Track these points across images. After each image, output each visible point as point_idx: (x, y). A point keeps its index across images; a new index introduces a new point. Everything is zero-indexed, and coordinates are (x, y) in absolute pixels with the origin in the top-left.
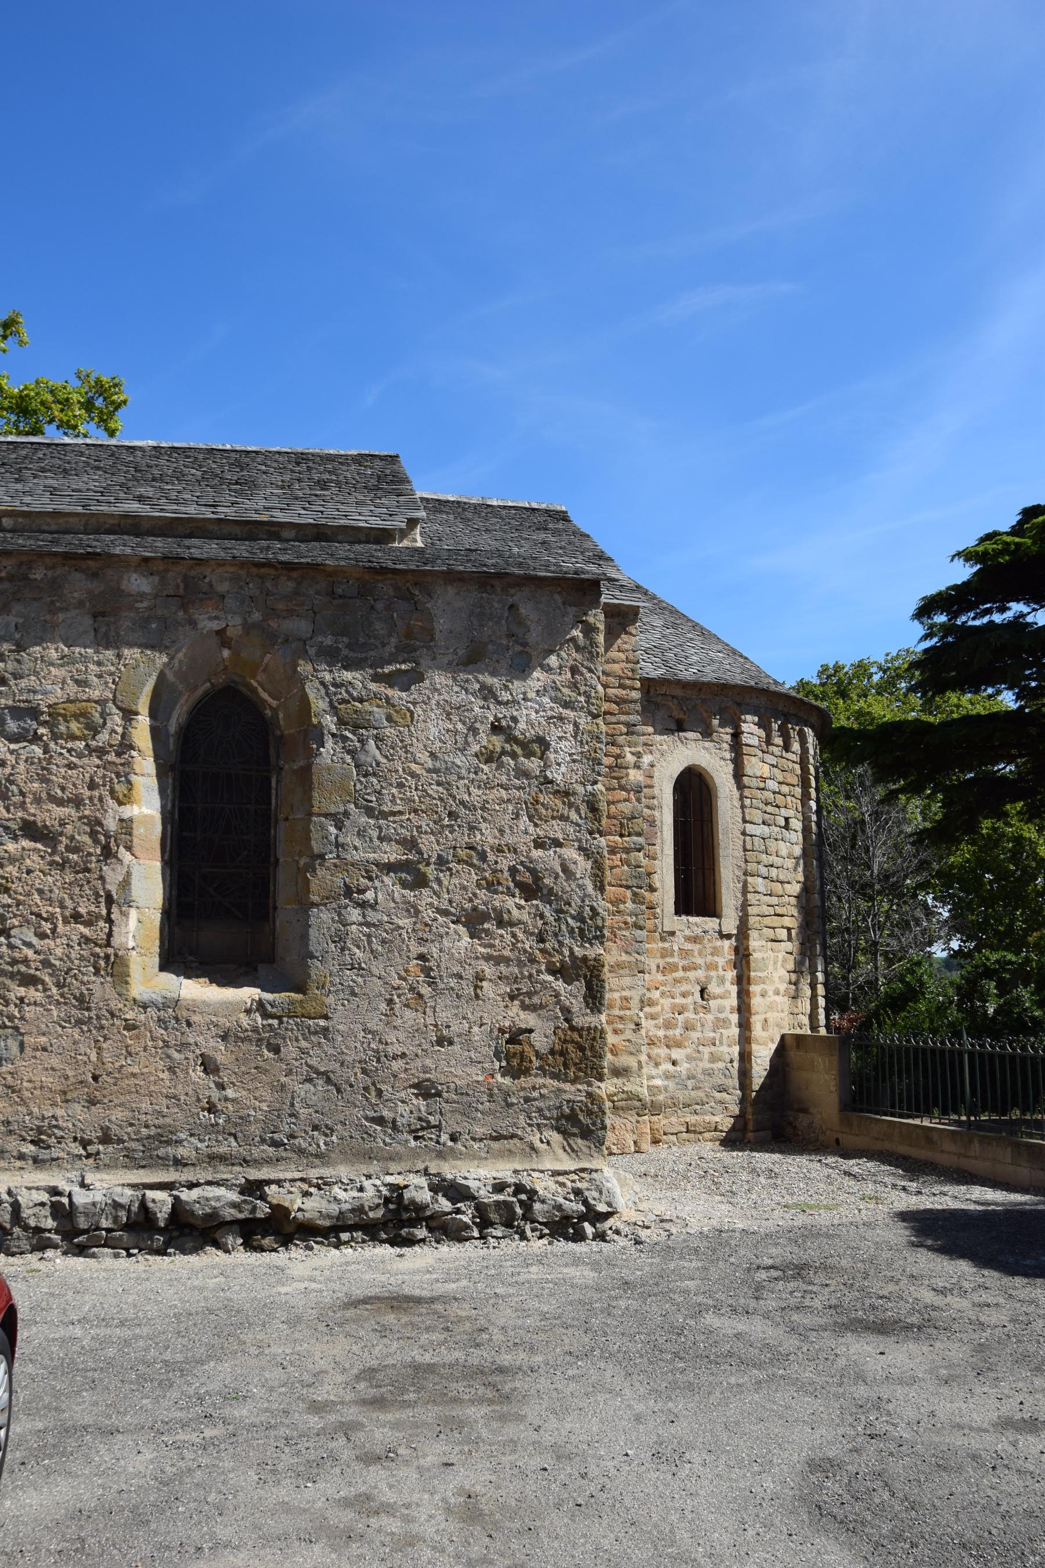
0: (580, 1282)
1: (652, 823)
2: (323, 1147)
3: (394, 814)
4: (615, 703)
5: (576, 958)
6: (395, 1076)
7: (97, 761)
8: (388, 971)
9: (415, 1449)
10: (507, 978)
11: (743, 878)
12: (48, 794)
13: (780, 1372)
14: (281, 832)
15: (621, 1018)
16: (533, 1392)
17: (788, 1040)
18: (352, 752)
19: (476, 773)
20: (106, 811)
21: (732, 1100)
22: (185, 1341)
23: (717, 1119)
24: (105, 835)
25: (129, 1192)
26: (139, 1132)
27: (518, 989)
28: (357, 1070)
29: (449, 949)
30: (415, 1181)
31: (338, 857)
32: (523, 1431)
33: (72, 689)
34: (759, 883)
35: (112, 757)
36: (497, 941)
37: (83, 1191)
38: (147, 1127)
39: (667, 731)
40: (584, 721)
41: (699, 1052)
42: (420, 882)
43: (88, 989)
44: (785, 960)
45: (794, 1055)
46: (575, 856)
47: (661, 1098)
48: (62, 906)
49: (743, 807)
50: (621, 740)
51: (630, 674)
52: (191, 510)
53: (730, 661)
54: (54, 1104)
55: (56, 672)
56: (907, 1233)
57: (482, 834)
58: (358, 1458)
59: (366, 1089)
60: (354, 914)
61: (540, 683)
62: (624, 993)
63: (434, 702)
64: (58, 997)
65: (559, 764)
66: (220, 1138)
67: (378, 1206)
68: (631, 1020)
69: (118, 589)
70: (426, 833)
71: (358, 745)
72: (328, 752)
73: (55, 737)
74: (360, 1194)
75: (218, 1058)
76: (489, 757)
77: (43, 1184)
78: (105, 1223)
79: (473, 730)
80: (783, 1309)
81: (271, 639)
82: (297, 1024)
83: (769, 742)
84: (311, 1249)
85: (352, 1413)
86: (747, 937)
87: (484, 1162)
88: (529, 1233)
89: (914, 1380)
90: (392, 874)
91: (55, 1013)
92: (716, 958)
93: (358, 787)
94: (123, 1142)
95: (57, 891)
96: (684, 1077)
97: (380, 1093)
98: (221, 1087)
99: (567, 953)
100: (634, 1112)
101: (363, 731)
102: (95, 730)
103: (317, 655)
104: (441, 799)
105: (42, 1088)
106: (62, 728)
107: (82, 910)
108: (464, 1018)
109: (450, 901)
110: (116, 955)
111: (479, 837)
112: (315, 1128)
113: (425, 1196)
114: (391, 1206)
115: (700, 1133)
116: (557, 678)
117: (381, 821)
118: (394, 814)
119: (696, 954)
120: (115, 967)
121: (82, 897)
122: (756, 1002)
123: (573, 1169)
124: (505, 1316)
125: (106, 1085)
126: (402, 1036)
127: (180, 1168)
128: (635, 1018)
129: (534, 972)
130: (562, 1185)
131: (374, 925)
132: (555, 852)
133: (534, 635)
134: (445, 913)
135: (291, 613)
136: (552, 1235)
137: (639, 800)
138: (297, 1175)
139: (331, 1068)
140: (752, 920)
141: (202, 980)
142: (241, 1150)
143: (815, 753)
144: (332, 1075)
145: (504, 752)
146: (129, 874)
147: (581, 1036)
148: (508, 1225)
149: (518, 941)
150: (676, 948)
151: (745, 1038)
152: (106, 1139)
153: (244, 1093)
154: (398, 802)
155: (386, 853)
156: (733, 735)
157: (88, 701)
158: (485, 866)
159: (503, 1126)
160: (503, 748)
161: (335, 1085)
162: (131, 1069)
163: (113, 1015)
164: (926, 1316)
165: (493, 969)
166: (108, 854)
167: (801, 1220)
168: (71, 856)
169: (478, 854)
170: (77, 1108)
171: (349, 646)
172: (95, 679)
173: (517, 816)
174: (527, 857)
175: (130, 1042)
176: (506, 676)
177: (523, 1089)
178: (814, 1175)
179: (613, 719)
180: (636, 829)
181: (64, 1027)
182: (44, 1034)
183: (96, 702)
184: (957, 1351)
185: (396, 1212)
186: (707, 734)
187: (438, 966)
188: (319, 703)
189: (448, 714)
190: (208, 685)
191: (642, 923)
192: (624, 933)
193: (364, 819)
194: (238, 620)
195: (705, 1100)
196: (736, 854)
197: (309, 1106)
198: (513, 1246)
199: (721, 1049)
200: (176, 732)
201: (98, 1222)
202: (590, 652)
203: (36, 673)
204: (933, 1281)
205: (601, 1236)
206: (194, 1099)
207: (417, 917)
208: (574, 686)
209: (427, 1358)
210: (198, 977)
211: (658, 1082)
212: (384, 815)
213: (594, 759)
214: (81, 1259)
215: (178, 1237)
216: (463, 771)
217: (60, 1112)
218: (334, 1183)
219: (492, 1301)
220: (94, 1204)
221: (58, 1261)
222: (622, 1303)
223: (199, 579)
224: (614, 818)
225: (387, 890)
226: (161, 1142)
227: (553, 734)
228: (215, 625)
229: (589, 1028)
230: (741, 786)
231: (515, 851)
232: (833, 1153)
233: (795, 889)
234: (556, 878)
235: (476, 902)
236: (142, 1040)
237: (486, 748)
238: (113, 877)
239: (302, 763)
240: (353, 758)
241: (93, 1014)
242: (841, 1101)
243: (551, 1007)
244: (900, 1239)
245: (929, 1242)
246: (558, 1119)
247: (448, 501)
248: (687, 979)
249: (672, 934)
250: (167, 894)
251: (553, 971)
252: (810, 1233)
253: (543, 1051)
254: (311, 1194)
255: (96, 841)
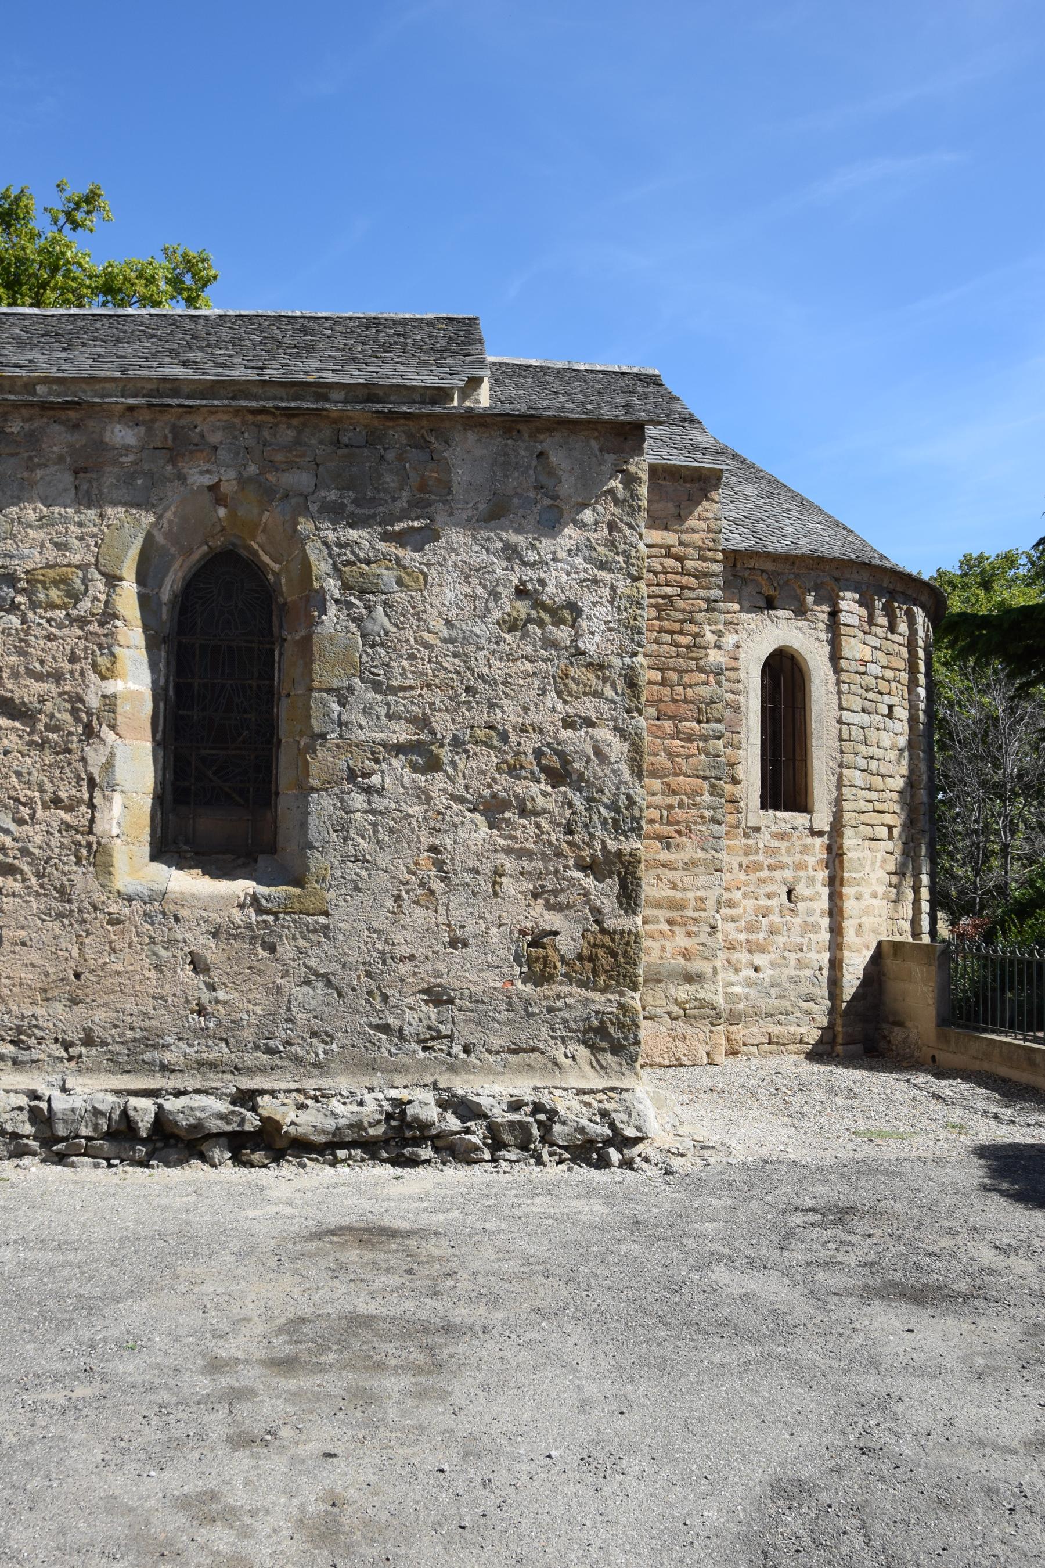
0: (585, 1218)
1: (737, 709)
2: (322, 1056)
3: (404, 689)
4: (694, 576)
5: (609, 852)
6: (402, 980)
7: (79, 632)
8: (395, 864)
9: (300, 1430)
10: (530, 873)
11: (838, 770)
12: (26, 668)
13: (779, 1349)
14: (284, 709)
15: (695, 920)
16: (474, 1360)
17: (885, 948)
18: (358, 620)
19: (497, 643)
20: (87, 686)
21: (821, 1012)
22: (113, 1271)
23: (803, 1030)
24: (87, 713)
25: (111, 1098)
26: (123, 1035)
27: (542, 887)
28: (360, 972)
29: (465, 840)
30: (420, 1097)
31: (341, 736)
32: (438, 1414)
33: (51, 553)
34: (855, 776)
35: (94, 627)
36: (519, 833)
37: (64, 1095)
38: (132, 1029)
39: (756, 609)
40: (622, 584)
41: (784, 958)
42: (433, 765)
43: (69, 880)
44: (884, 861)
45: (891, 964)
46: (609, 737)
47: (741, 1006)
48: (42, 791)
49: (839, 692)
50: (700, 617)
51: (711, 545)
52: (236, 373)
53: (831, 532)
54: (34, 1003)
55: (35, 534)
56: (981, 1174)
57: (503, 712)
58: (229, 1439)
59: (370, 993)
60: (359, 801)
61: (572, 542)
62: (699, 893)
63: (450, 563)
64: (38, 888)
65: (592, 633)
66: (211, 1043)
67: (379, 1122)
68: (706, 922)
69: (102, 442)
70: (440, 710)
71: (364, 612)
72: (331, 620)
73: (34, 605)
74: (360, 1109)
75: (209, 957)
76: (513, 625)
77: (22, 1087)
78: (84, 1131)
79: (495, 595)
80: (809, 1264)
81: (268, 494)
82: (294, 921)
83: (871, 622)
84: (303, 1166)
85: (249, 1376)
86: (841, 835)
87: (501, 1077)
88: (546, 1158)
89: (941, 1371)
90: (401, 756)
91: (35, 905)
92: (806, 857)
93: (364, 659)
94: (107, 1045)
95: (36, 774)
96: (767, 985)
97: (385, 998)
98: (212, 988)
99: (599, 847)
100: (707, 1021)
101: (370, 597)
102: (76, 598)
103: (320, 511)
104: (457, 673)
105: (21, 985)
106: (41, 596)
107: (63, 795)
108: (480, 917)
109: (467, 787)
110: (99, 843)
111: (500, 715)
112: (314, 1034)
113: (432, 1113)
114: (393, 1123)
115: (784, 1045)
116: (591, 535)
117: (389, 697)
118: (404, 689)
119: (783, 852)
120: (96, 856)
121: (62, 779)
122: (850, 905)
123: (600, 1088)
124: (483, 1258)
125: (88, 983)
126: (410, 936)
127: (167, 1074)
128: (711, 921)
129: (561, 867)
130: (588, 1105)
131: (381, 813)
132: (587, 733)
133: (567, 487)
134: (461, 800)
135: (290, 465)
136: (573, 1160)
137: (719, 683)
138: (293, 1086)
139: (332, 970)
140: (847, 817)
141: (194, 871)
142: (233, 1056)
143: (927, 636)
144: (332, 978)
145: (529, 620)
146: (112, 755)
147: (613, 941)
148: (524, 1147)
149: (542, 833)
150: (761, 845)
151: (836, 945)
152: (88, 1041)
153: (237, 995)
154: (409, 675)
155: (394, 732)
156: (830, 614)
157: (69, 565)
158: (507, 748)
159: (523, 1038)
160: (529, 615)
161: (336, 988)
162: (115, 967)
163: (95, 908)
164: (979, 1282)
165: (515, 863)
166: (90, 732)
167: (866, 1151)
168: (51, 735)
169: (499, 734)
170: (58, 1007)
171: (356, 502)
172: (76, 542)
173: (544, 692)
174: (555, 738)
175: (114, 938)
176: (533, 533)
177: (546, 998)
178: (898, 1096)
179: (692, 594)
180: (716, 714)
181: (44, 921)
182: (23, 928)
183: (77, 567)
184: (1002, 1332)
185: (399, 1129)
186: (801, 611)
187: (452, 859)
188: (321, 566)
189: (467, 577)
190: (205, 548)
191: (720, 817)
192: (700, 828)
193: (370, 695)
194: (232, 474)
195: (790, 1009)
196: (831, 744)
197: (307, 1011)
198: (527, 1171)
199: (809, 955)
200: (170, 601)
201: (77, 1129)
202: (631, 506)
203: (13, 536)
204: (998, 1236)
205: (628, 1164)
206: (183, 1000)
207: (428, 804)
208: (612, 544)
209: (372, 1308)
210: (191, 868)
211: (738, 989)
212: (393, 690)
213: (633, 628)
214: (60, 1168)
215: (162, 1149)
216: (483, 641)
217: (40, 1011)
218: (333, 1096)
219: (476, 1238)
220: (73, 1110)
221: (33, 1169)
222: (624, 1248)
223: (190, 429)
224: (691, 702)
225: (395, 775)
226: (147, 1046)
227: (586, 599)
228: (207, 480)
229: (622, 932)
230: (837, 670)
231: (541, 731)
232: (928, 1071)
233: (899, 783)
234: (588, 762)
235: (496, 788)
236: (127, 936)
237: (509, 615)
238: (96, 757)
239: (303, 633)
240: (359, 626)
241: (74, 907)
242: (938, 1015)
243: (580, 907)
244: (971, 1180)
245: (1005, 1186)
246: (585, 1032)
247: (530, 366)
248: (772, 879)
249: (757, 830)
250: (160, 778)
251: (583, 868)
252: (869, 1168)
253: (569, 956)
254: (307, 1107)
255: (77, 720)
